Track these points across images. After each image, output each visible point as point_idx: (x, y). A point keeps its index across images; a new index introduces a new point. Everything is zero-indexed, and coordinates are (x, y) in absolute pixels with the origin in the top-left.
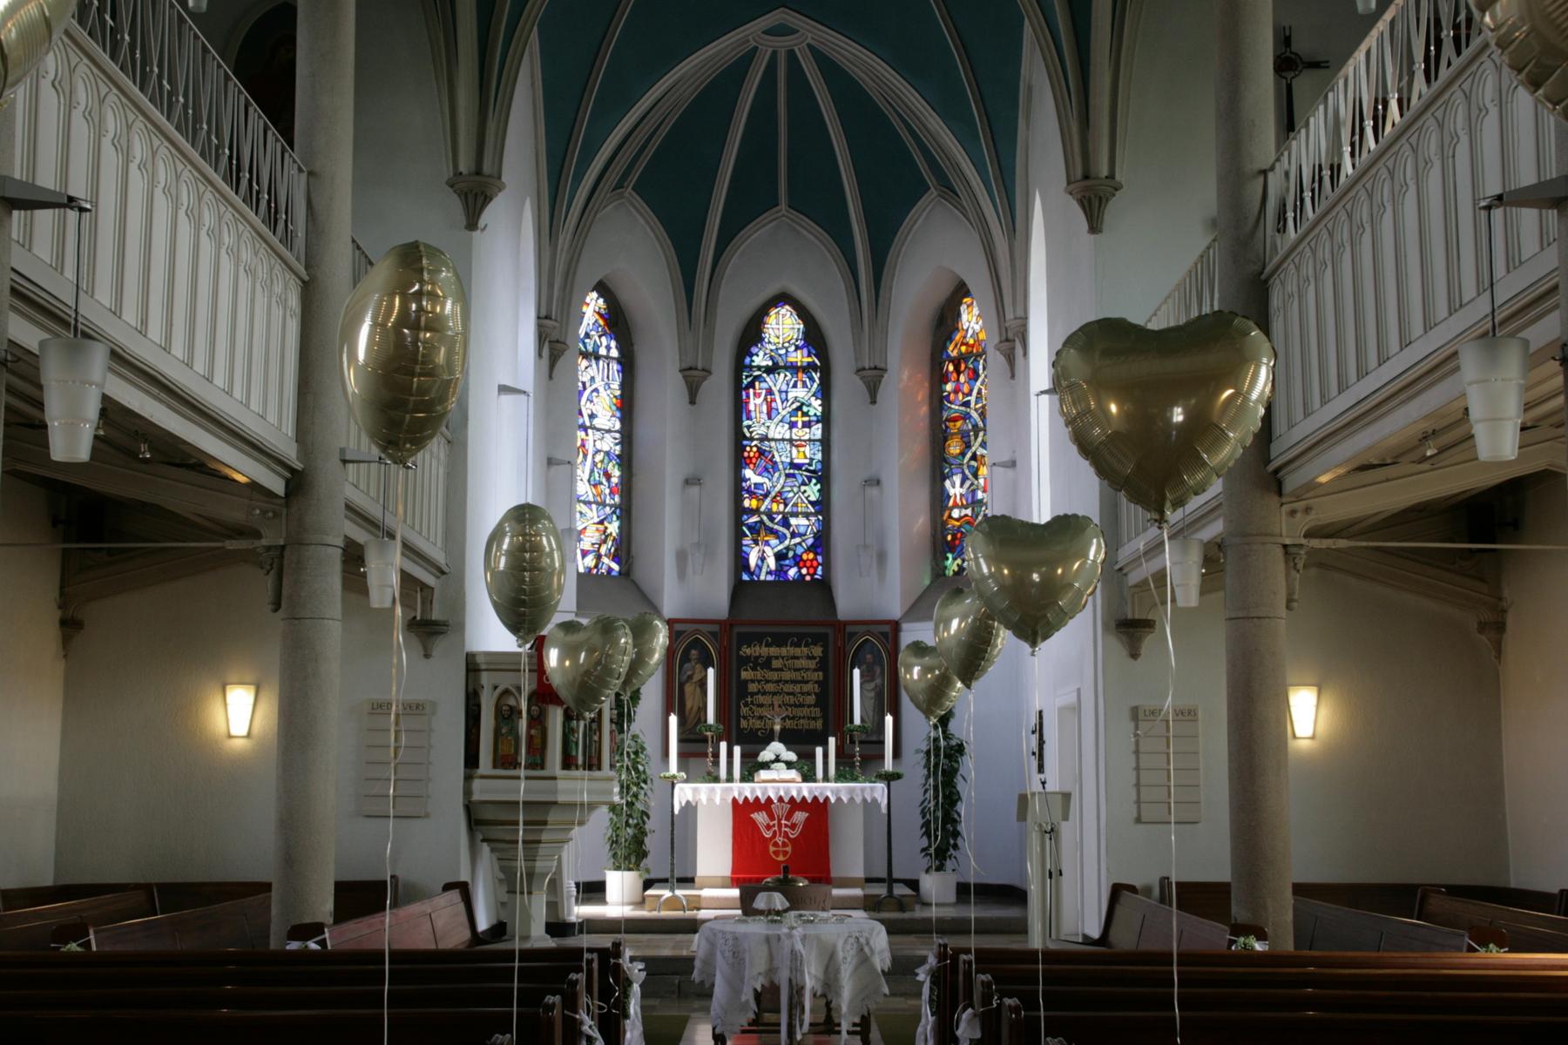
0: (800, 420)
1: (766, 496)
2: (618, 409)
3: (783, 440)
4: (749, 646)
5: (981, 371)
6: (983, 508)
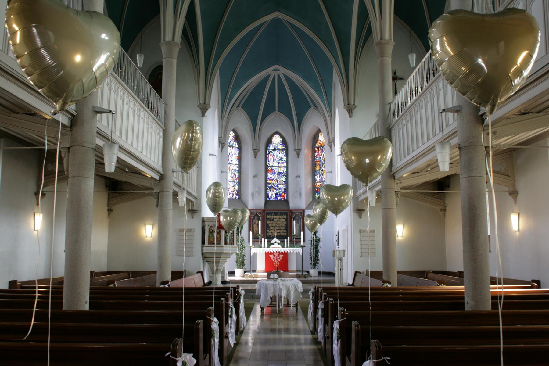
0: (281, 162)
1: (273, 180)
2: (238, 159)
3: (277, 166)
4: (269, 215)
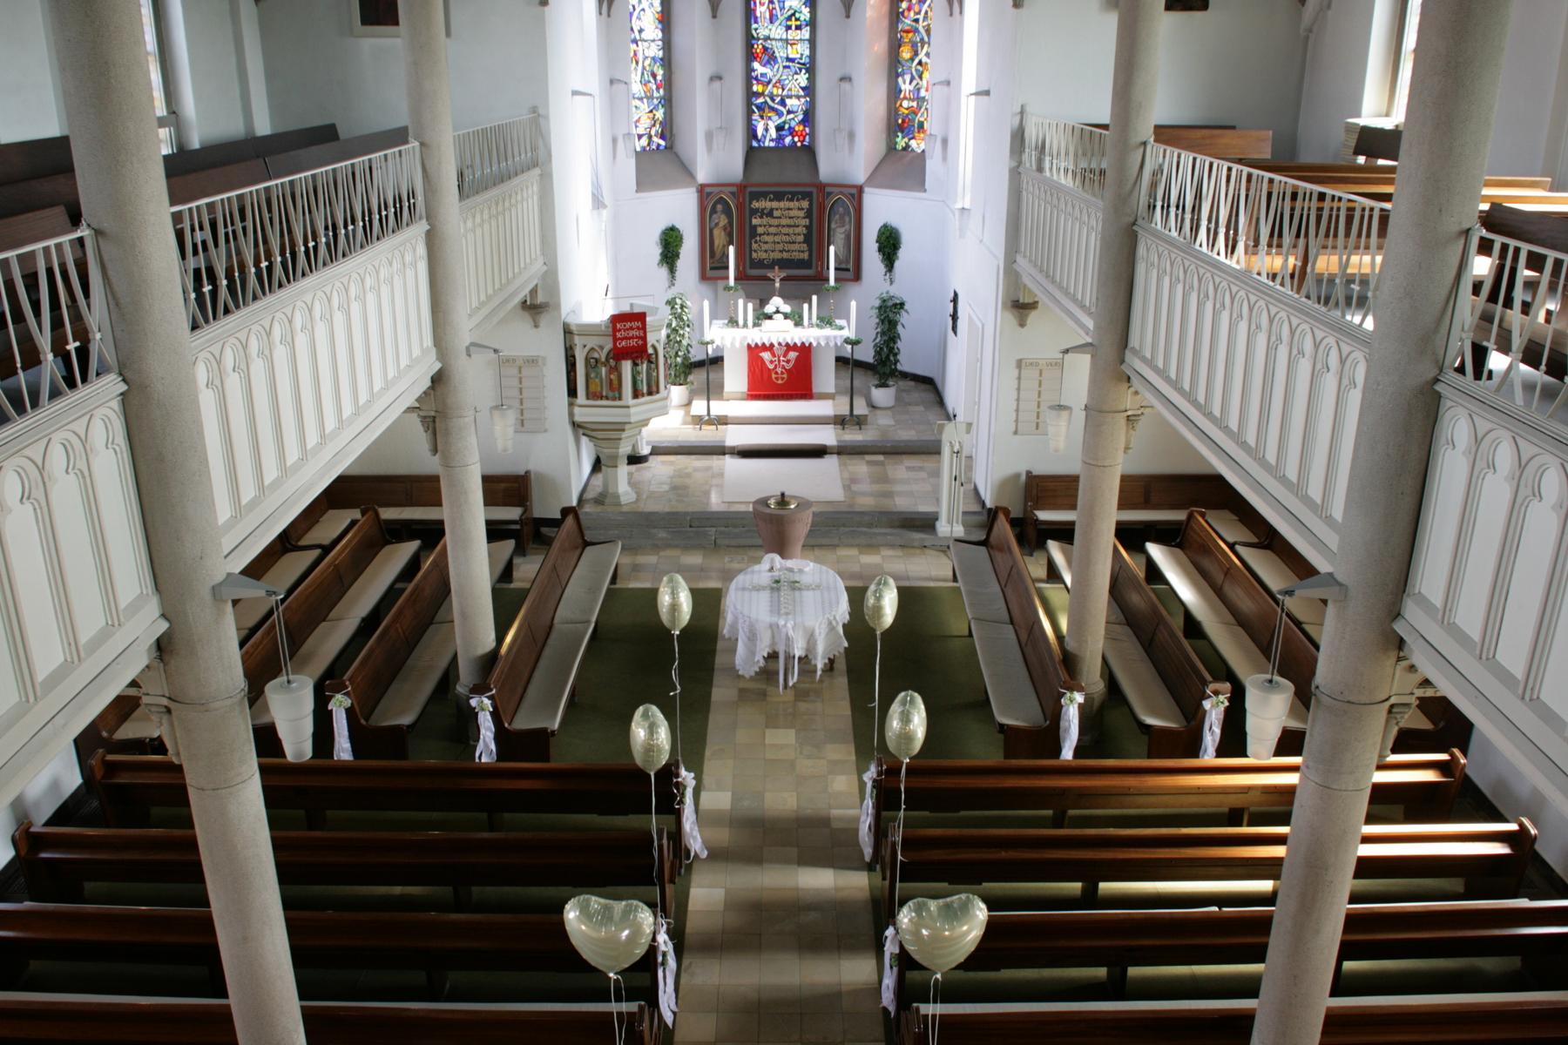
1: (769, 83)
2: (660, 22)
3: (781, 40)
4: (757, 201)
6: (925, 104)
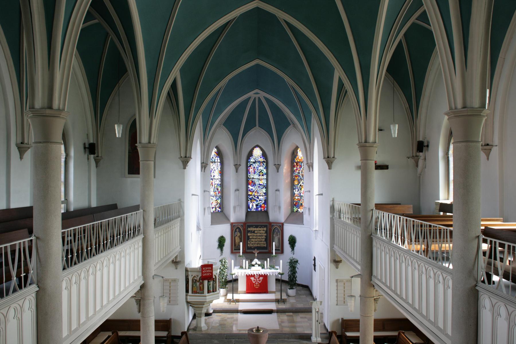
2: (220, 174)
3: (257, 179)
4: (250, 228)
5: (302, 166)
